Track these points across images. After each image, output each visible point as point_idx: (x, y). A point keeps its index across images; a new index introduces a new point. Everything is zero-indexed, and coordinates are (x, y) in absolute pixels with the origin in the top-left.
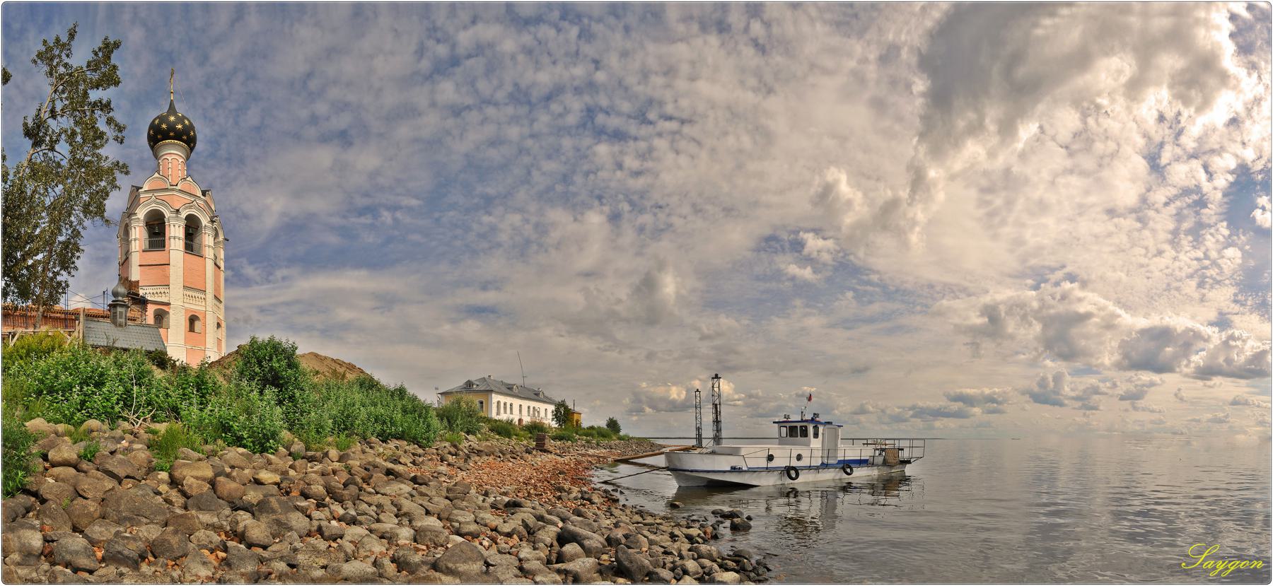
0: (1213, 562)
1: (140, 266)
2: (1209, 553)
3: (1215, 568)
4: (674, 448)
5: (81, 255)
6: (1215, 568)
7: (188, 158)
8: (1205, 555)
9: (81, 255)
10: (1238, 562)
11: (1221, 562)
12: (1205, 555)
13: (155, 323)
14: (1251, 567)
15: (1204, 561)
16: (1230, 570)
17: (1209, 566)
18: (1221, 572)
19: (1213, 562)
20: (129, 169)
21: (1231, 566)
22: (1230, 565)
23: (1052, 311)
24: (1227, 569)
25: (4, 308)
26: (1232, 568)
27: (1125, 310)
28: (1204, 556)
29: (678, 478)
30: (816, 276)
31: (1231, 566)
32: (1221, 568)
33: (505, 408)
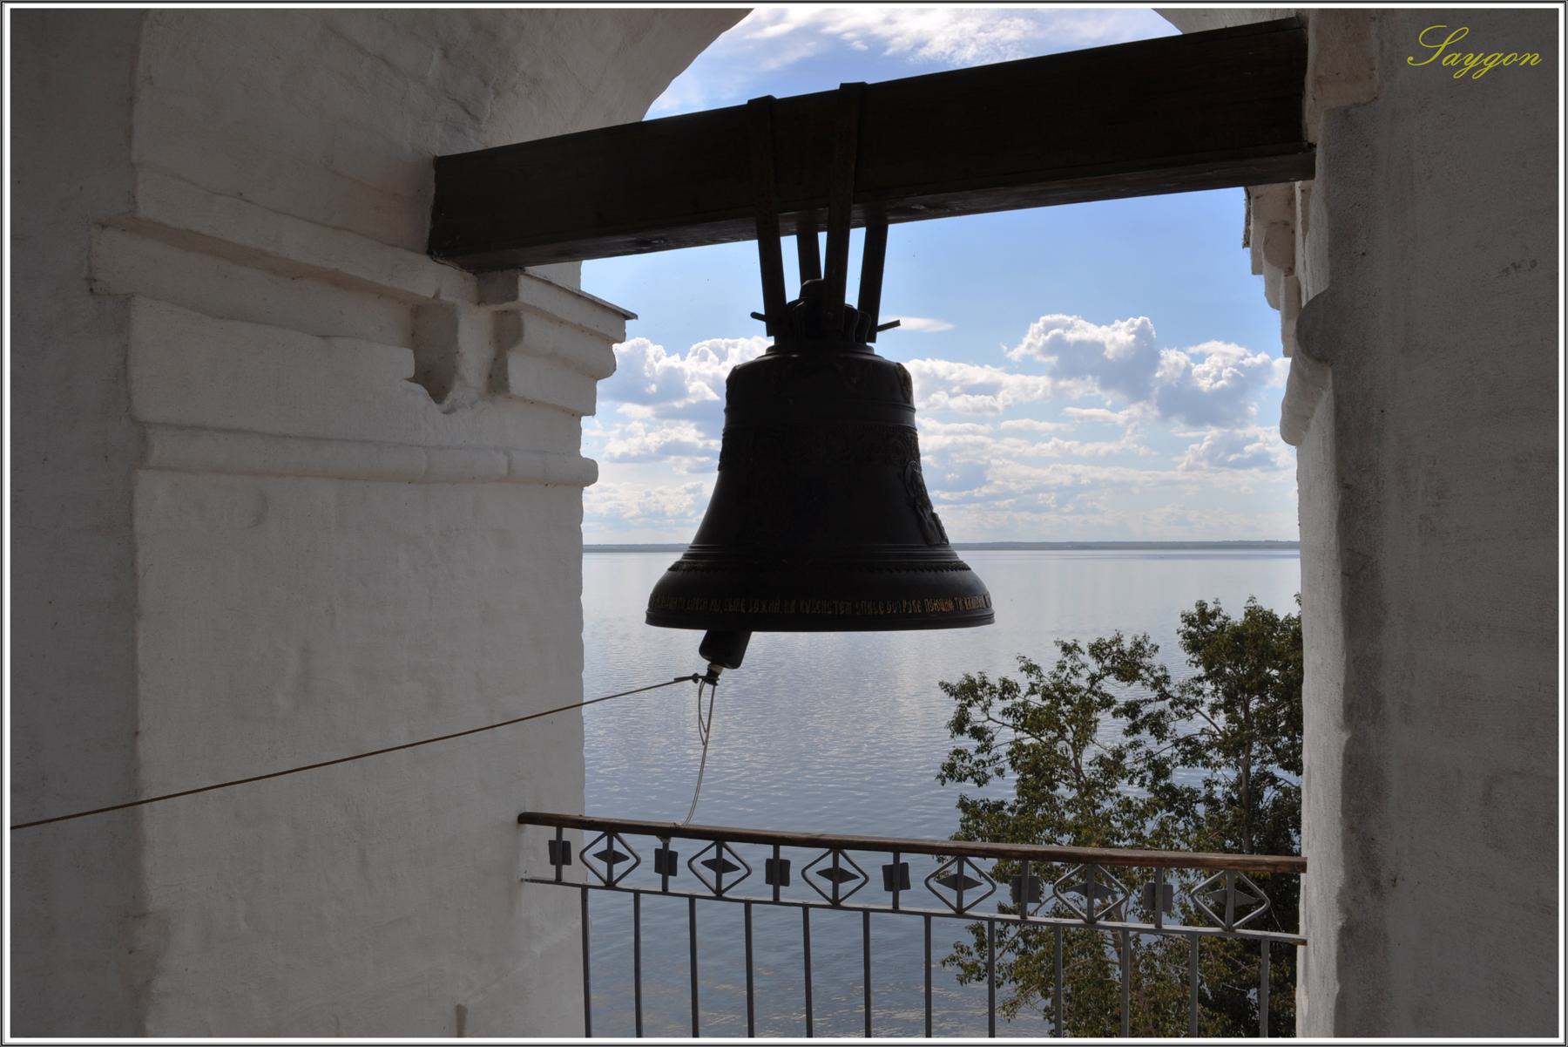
0: (1457, 56)
4: (702, 730)
5: (1151, 641)
6: (1461, 65)
8: (1446, 43)
9: (1151, 641)
11: (1472, 55)
12: (1446, 43)
13: (1296, 947)
15: (1447, 51)
16: (1486, 69)
18: (1473, 70)
19: (1457, 56)
20: (949, 708)
21: (1488, 62)
22: (1486, 60)
24: (1482, 66)
26: (1490, 65)
27: (936, 375)
28: (1443, 46)
29: (721, 876)
31: (1488, 62)
32: (1472, 65)
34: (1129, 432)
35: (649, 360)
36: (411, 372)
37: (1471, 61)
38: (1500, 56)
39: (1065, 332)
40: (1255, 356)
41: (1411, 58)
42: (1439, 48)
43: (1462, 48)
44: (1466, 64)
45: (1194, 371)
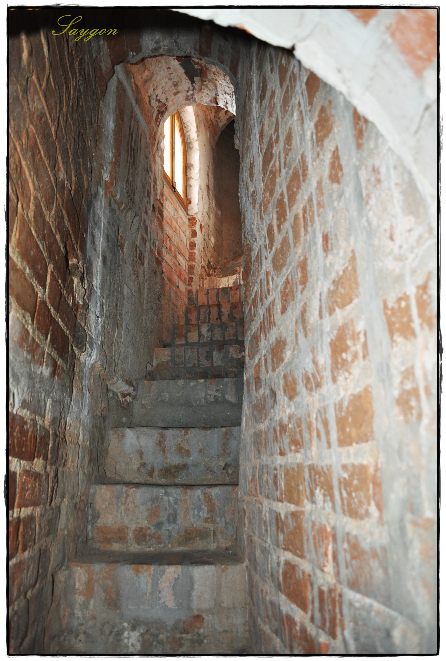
0: (77, 30)
8: (71, 24)
10: (97, 30)
12: (71, 24)
16: (91, 37)
17: (74, 33)
19: (77, 30)
21: (92, 33)
24: (89, 35)
26: (93, 35)
28: (70, 25)
31: (92, 33)
32: (84, 35)
34: (38, 494)
35: (285, 171)
36: (298, 53)
38: (97, 30)
39: (335, 585)
40: (371, 606)
41: (53, 31)
42: (67, 27)
43: (79, 26)
44: (80, 34)
45: (219, 339)
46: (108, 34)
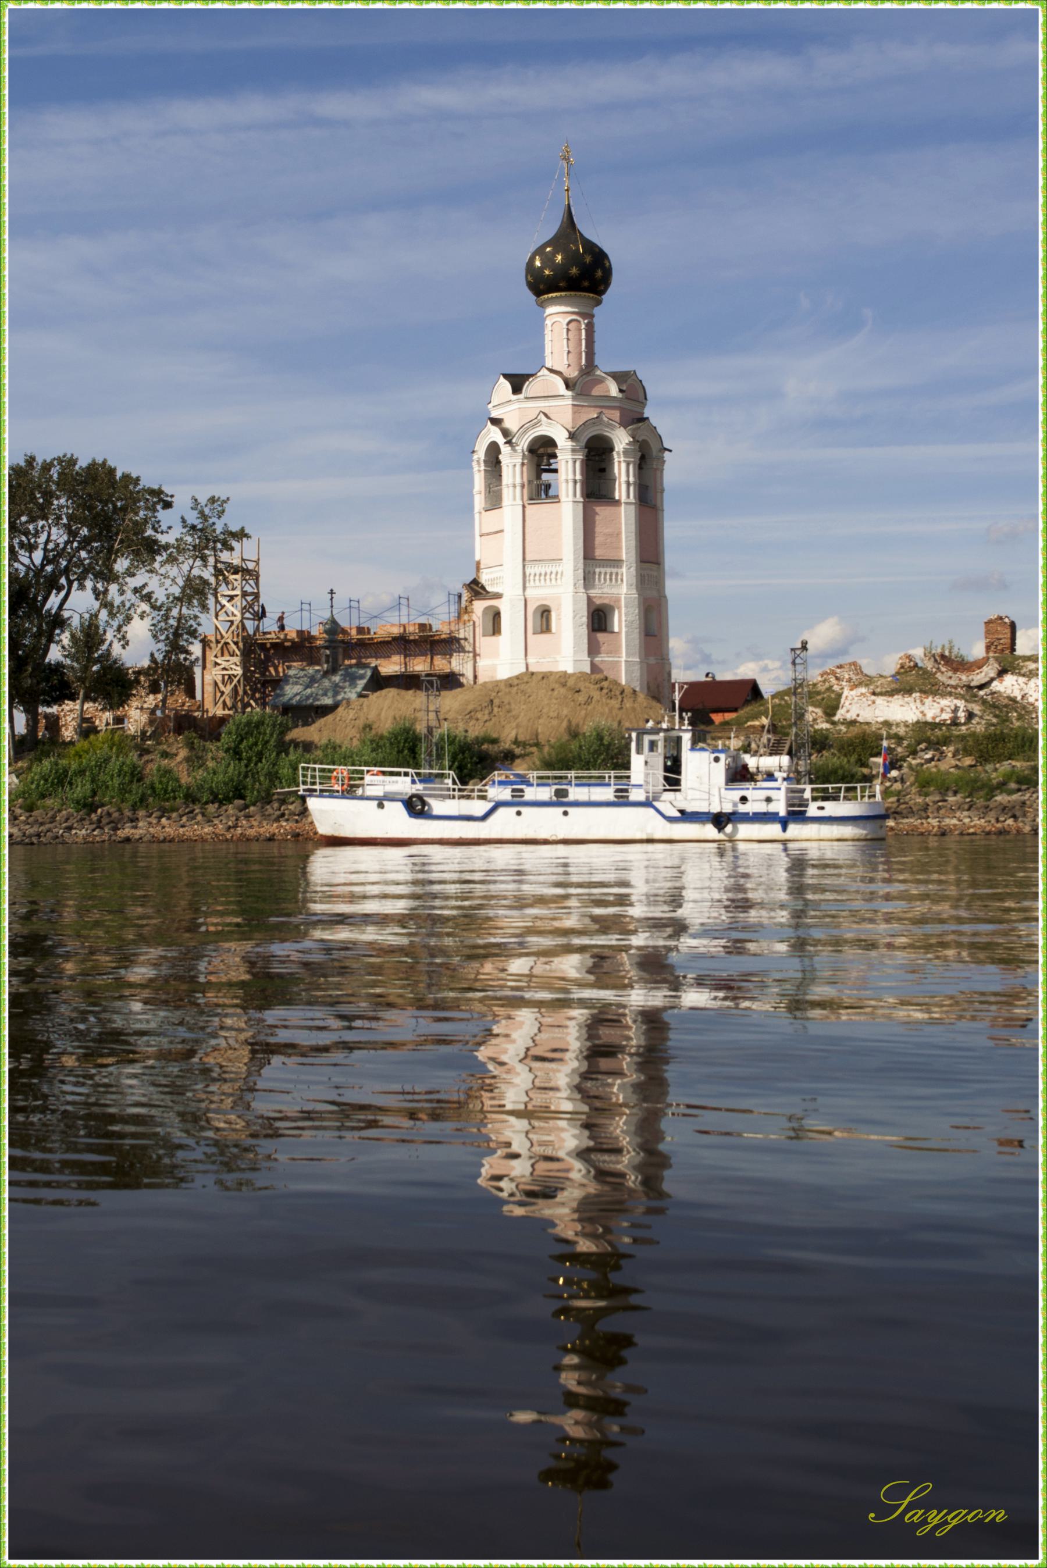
0: (921, 1512)
1: (502, 531)
2: (914, 1496)
3: (925, 1522)
6: (925, 1522)
7: (532, 375)
8: (908, 1499)
10: (964, 1512)
11: (936, 1512)
12: (908, 1499)
14: (987, 1521)
15: (910, 1507)
16: (950, 1526)
18: (936, 1527)
19: (921, 1512)
21: (952, 1519)
22: (950, 1517)
23: (114, 1025)
24: (946, 1523)
25: (13, 578)
26: (954, 1522)
28: (906, 1502)
30: (340, 673)
31: (952, 1519)
33: (622, 797)
37: (934, 1517)
38: (964, 1512)
41: (872, 1515)
46: (987, 1521)
